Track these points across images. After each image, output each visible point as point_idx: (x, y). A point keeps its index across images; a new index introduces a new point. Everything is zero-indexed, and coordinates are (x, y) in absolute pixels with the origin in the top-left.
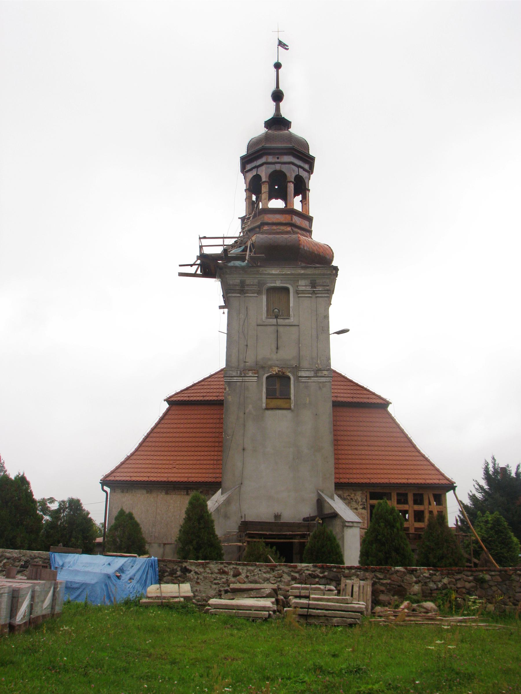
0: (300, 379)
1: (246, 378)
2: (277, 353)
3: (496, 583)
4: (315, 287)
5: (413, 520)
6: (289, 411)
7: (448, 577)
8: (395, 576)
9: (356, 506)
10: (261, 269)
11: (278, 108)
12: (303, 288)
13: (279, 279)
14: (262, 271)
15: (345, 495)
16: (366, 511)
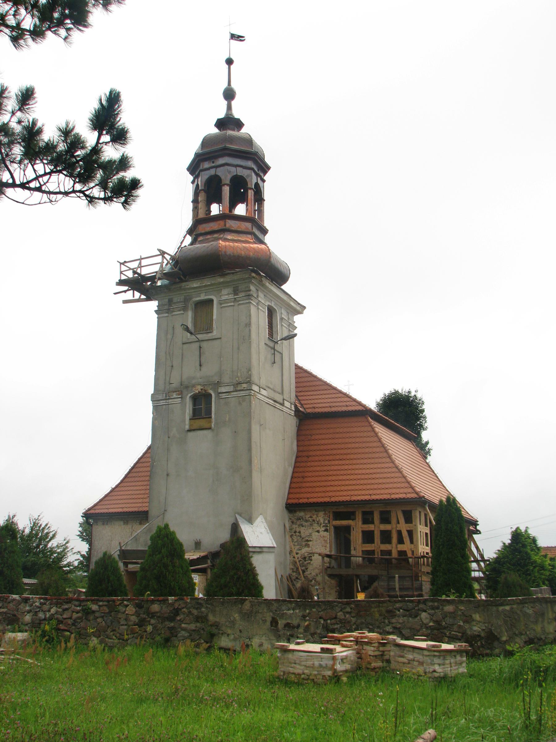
0: (220, 395)
1: (170, 401)
2: (200, 370)
3: (103, 614)
4: (237, 294)
5: (379, 542)
6: (209, 431)
7: (57, 607)
8: (11, 605)
9: (318, 528)
10: (184, 284)
11: (229, 108)
12: (226, 297)
13: (203, 292)
14: (185, 286)
15: (308, 516)
16: (328, 533)
